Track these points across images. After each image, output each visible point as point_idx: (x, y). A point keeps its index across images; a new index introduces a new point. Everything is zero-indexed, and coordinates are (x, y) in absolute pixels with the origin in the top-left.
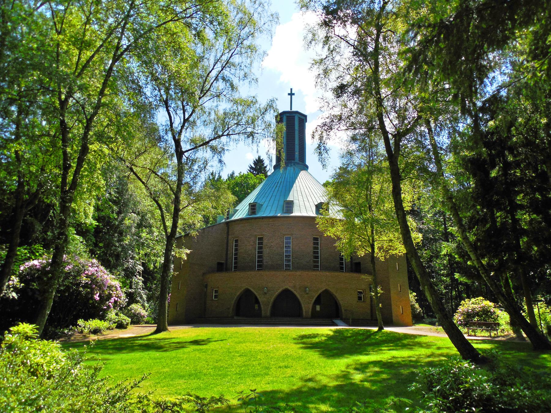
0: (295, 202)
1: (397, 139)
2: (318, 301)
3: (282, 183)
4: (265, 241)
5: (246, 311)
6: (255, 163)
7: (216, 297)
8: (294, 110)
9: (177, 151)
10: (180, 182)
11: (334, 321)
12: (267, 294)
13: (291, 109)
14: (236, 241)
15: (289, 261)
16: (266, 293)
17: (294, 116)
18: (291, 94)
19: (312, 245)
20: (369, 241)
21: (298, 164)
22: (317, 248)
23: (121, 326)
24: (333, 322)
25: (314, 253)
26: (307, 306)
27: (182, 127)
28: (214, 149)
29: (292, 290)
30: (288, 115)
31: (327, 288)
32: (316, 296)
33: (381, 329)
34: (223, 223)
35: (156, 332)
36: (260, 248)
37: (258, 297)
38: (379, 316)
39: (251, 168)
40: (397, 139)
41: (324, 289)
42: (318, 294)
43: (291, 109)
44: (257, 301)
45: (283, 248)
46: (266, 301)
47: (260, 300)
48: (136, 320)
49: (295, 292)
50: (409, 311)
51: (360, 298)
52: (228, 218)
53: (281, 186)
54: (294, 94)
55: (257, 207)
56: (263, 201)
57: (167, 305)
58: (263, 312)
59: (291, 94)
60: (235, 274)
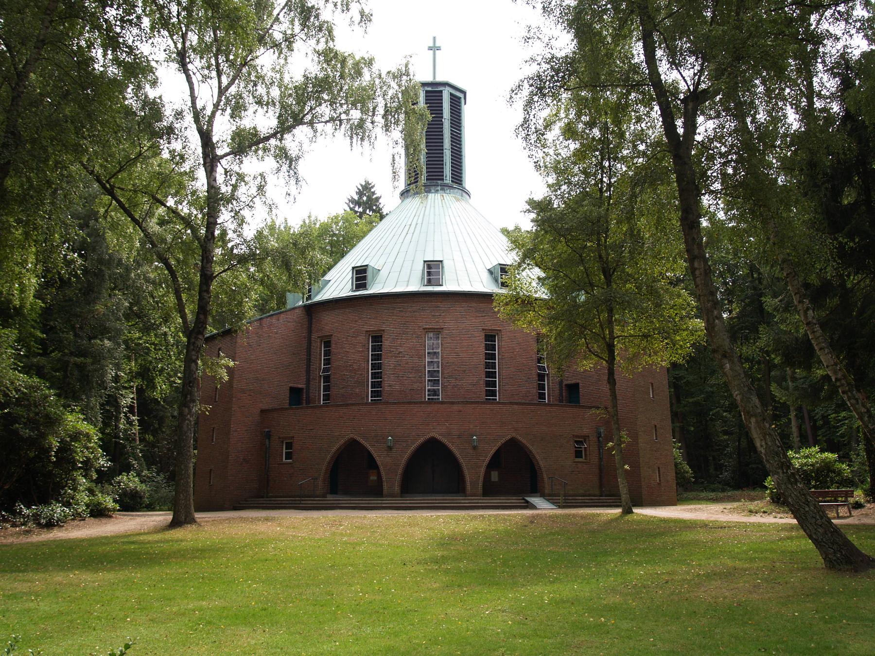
0: (445, 263)
1: (690, 107)
2: (495, 463)
3: (419, 226)
4: (386, 343)
5: (351, 479)
6: (360, 193)
7: (289, 456)
8: (439, 79)
9: (205, 155)
10: (212, 220)
11: (528, 499)
12: (394, 450)
13: (434, 78)
14: (328, 344)
15: (436, 382)
16: (390, 448)
17: (441, 92)
18: (434, 48)
19: (482, 350)
20: (604, 338)
21: (451, 187)
22: (493, 356)
23: (98, 513)
24: (527, 502)
25: (487, 365)
26: (474, 471)
27: (216, 106)
28: (283, 154)
29: (445, 441)
30: (429, 89)
31: (514, 435)
32: (492, 452)
33: (628, 511)
34: (299, 307)
35: (175, 524)
36: (376, 357)
37: (375, 455)
38: (623, 490)
39: (352, 201)
40: (690, 107)
41: (509, 437)
42: (496, 448)
43: (434, 78)
44: (372, 464)
45: (421, 357)
46: (391, 464)
47: (378, 459)
48: (130, 503)
49: (450, 445)
50: (671, 476)
51: (578, 454)
52: (307, 299)
53: (417, 231)
54: (439, 49)
55: (369, 274)
56: (381, 262)
57: (191, 471)
58: (385, 484)
59: (434, 48)
60: (324, 407)
